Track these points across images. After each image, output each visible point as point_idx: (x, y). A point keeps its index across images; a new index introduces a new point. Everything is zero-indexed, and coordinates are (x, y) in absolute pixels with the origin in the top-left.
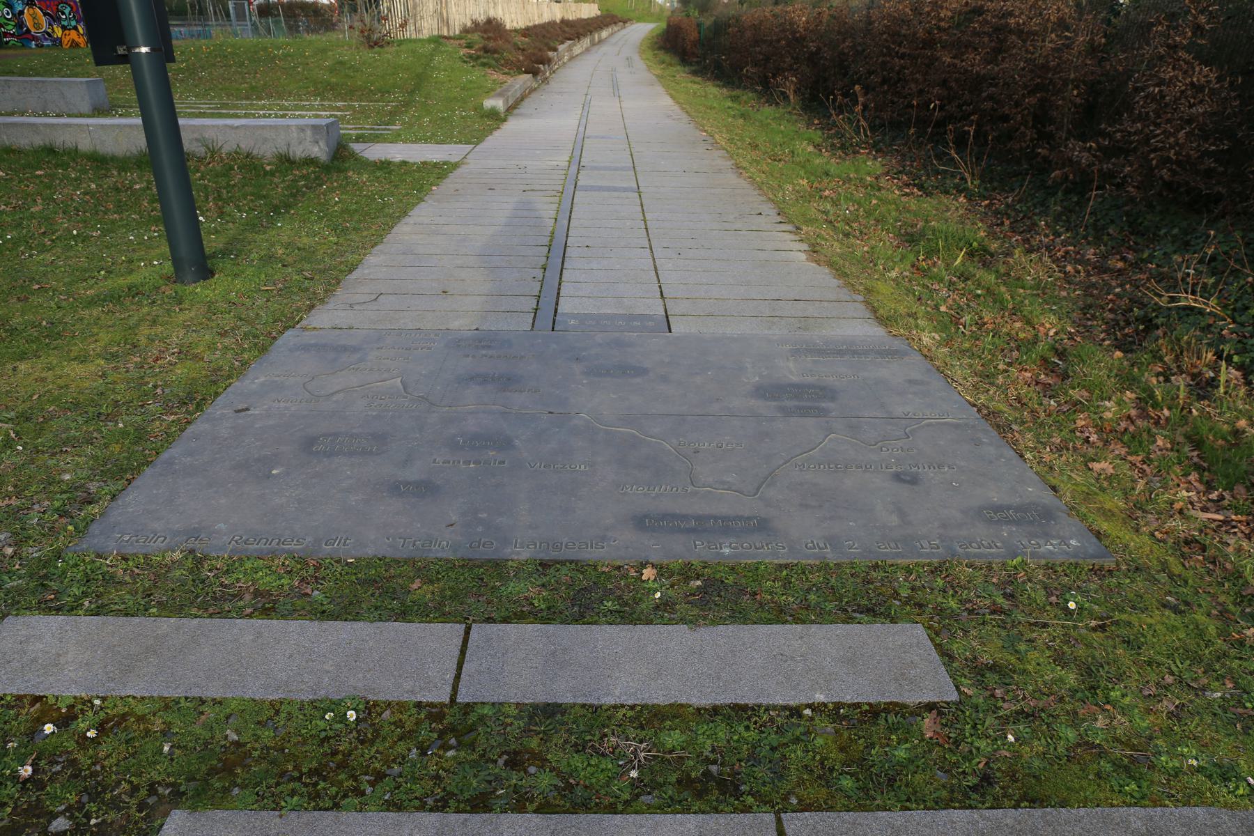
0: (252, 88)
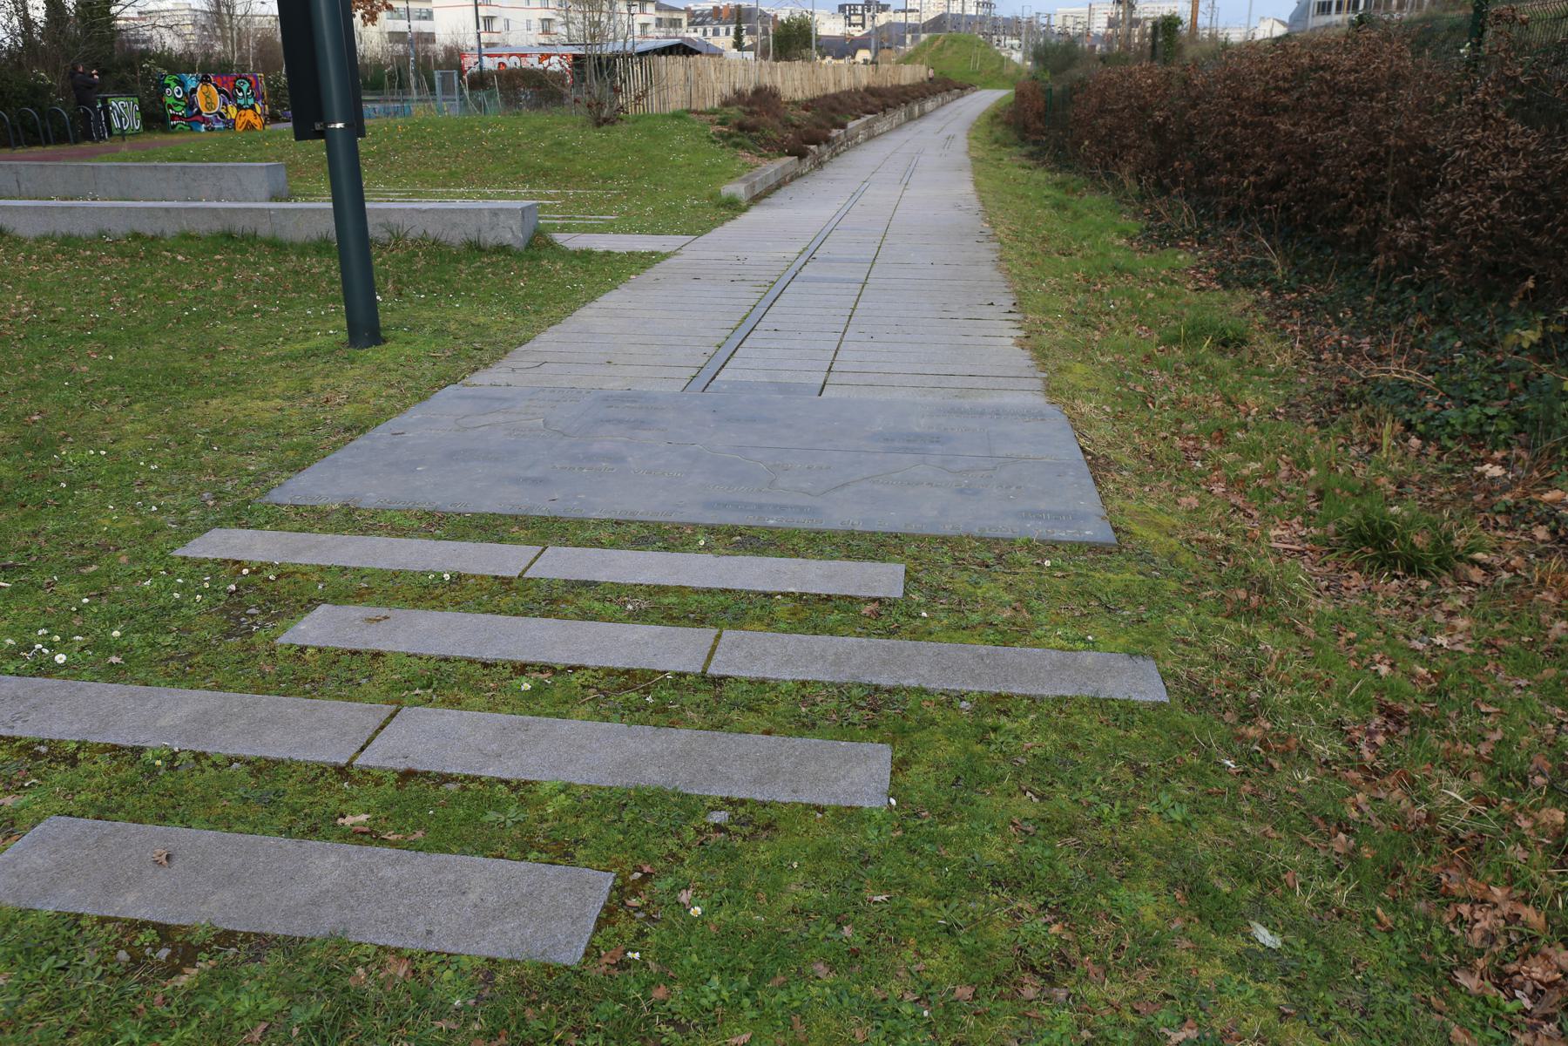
0: (452, 174)
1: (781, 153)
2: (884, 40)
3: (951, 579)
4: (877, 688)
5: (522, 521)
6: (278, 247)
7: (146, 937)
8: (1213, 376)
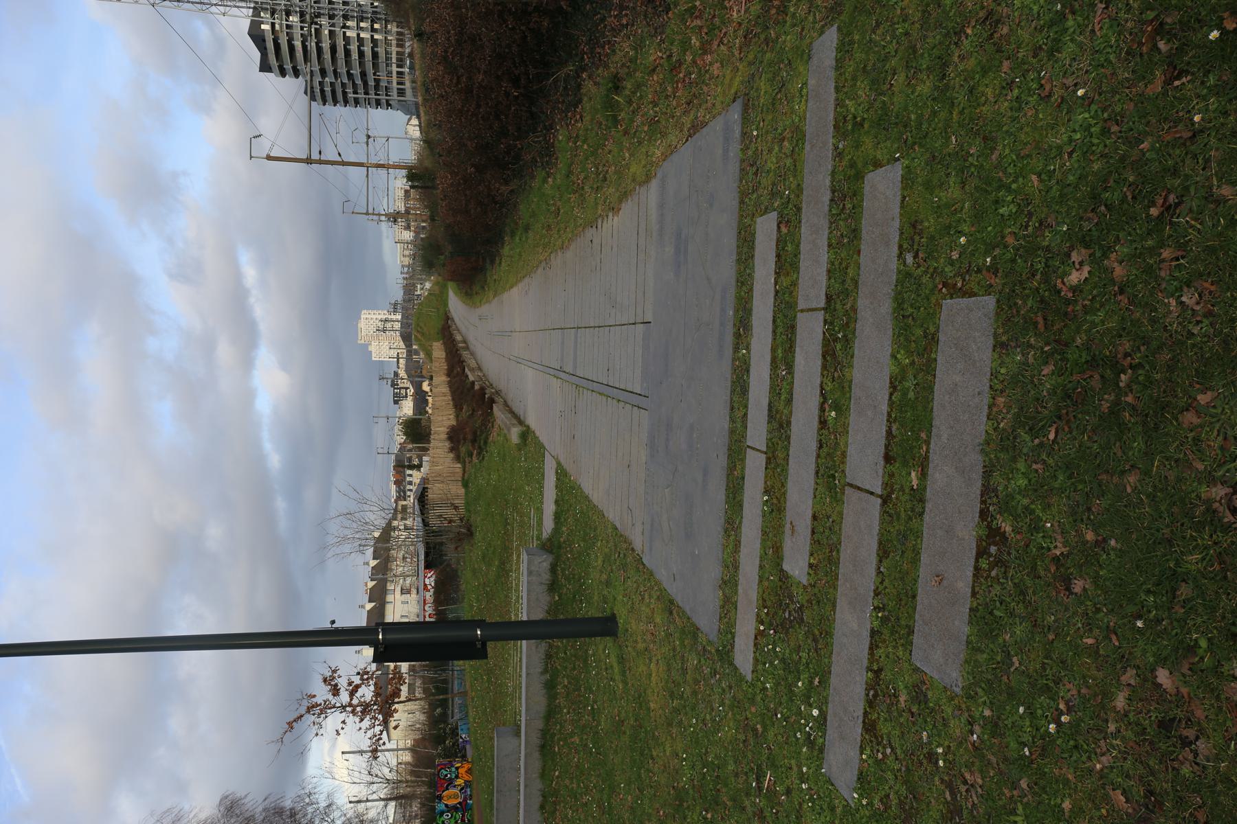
1: (492, 413)
2: (416, 374)
3: (765, 187)
4: (832, 200)
5: (731, 468)
6: (551, 714)
7: (984, 564)
8: (638, 86)
